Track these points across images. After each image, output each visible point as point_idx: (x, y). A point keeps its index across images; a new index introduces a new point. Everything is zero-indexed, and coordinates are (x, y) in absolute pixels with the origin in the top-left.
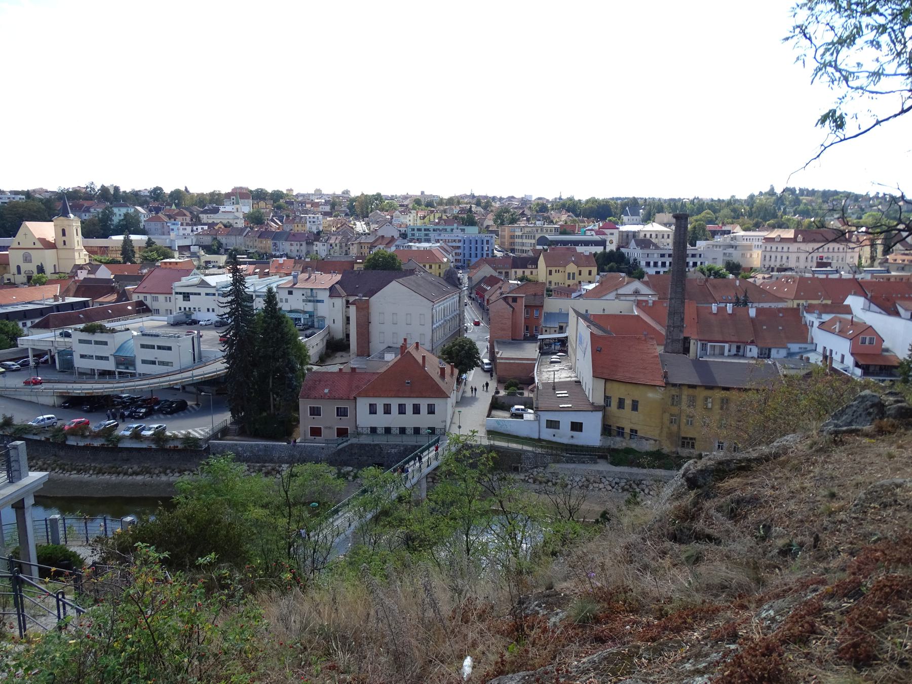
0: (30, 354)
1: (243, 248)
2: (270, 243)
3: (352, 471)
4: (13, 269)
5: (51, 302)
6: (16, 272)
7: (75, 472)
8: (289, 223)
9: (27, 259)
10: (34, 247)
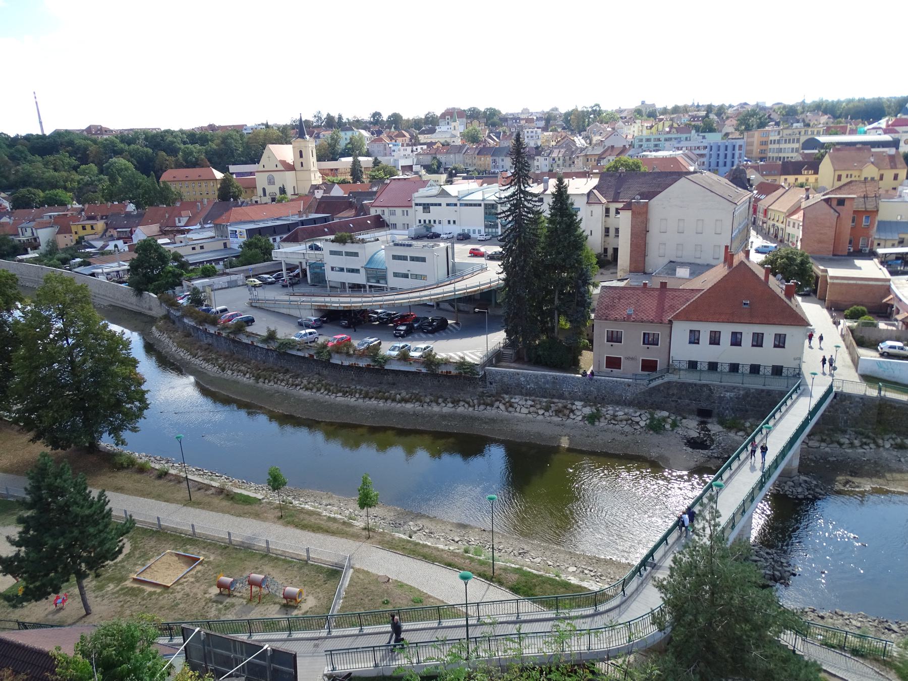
0: (284, 268)
1: (463, 167)
2: (489, 159)
3: (669, 417)
4: (260, 192)
5: (296, 218)
6: (262, 195)
7: (341, 394)
8: (506, 139)
9: (271, 182)
10: (276, 169)
